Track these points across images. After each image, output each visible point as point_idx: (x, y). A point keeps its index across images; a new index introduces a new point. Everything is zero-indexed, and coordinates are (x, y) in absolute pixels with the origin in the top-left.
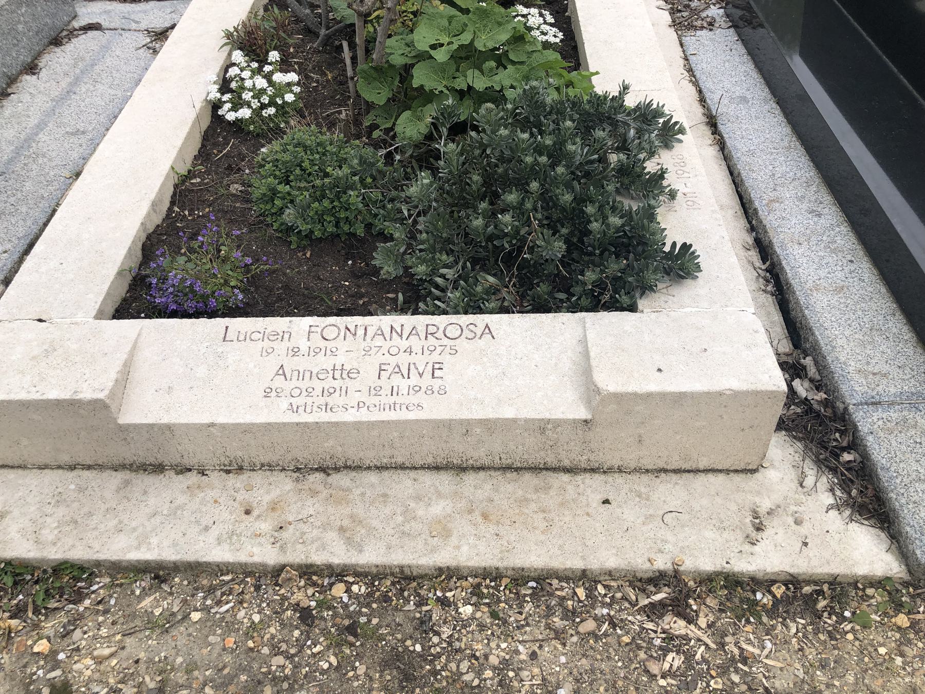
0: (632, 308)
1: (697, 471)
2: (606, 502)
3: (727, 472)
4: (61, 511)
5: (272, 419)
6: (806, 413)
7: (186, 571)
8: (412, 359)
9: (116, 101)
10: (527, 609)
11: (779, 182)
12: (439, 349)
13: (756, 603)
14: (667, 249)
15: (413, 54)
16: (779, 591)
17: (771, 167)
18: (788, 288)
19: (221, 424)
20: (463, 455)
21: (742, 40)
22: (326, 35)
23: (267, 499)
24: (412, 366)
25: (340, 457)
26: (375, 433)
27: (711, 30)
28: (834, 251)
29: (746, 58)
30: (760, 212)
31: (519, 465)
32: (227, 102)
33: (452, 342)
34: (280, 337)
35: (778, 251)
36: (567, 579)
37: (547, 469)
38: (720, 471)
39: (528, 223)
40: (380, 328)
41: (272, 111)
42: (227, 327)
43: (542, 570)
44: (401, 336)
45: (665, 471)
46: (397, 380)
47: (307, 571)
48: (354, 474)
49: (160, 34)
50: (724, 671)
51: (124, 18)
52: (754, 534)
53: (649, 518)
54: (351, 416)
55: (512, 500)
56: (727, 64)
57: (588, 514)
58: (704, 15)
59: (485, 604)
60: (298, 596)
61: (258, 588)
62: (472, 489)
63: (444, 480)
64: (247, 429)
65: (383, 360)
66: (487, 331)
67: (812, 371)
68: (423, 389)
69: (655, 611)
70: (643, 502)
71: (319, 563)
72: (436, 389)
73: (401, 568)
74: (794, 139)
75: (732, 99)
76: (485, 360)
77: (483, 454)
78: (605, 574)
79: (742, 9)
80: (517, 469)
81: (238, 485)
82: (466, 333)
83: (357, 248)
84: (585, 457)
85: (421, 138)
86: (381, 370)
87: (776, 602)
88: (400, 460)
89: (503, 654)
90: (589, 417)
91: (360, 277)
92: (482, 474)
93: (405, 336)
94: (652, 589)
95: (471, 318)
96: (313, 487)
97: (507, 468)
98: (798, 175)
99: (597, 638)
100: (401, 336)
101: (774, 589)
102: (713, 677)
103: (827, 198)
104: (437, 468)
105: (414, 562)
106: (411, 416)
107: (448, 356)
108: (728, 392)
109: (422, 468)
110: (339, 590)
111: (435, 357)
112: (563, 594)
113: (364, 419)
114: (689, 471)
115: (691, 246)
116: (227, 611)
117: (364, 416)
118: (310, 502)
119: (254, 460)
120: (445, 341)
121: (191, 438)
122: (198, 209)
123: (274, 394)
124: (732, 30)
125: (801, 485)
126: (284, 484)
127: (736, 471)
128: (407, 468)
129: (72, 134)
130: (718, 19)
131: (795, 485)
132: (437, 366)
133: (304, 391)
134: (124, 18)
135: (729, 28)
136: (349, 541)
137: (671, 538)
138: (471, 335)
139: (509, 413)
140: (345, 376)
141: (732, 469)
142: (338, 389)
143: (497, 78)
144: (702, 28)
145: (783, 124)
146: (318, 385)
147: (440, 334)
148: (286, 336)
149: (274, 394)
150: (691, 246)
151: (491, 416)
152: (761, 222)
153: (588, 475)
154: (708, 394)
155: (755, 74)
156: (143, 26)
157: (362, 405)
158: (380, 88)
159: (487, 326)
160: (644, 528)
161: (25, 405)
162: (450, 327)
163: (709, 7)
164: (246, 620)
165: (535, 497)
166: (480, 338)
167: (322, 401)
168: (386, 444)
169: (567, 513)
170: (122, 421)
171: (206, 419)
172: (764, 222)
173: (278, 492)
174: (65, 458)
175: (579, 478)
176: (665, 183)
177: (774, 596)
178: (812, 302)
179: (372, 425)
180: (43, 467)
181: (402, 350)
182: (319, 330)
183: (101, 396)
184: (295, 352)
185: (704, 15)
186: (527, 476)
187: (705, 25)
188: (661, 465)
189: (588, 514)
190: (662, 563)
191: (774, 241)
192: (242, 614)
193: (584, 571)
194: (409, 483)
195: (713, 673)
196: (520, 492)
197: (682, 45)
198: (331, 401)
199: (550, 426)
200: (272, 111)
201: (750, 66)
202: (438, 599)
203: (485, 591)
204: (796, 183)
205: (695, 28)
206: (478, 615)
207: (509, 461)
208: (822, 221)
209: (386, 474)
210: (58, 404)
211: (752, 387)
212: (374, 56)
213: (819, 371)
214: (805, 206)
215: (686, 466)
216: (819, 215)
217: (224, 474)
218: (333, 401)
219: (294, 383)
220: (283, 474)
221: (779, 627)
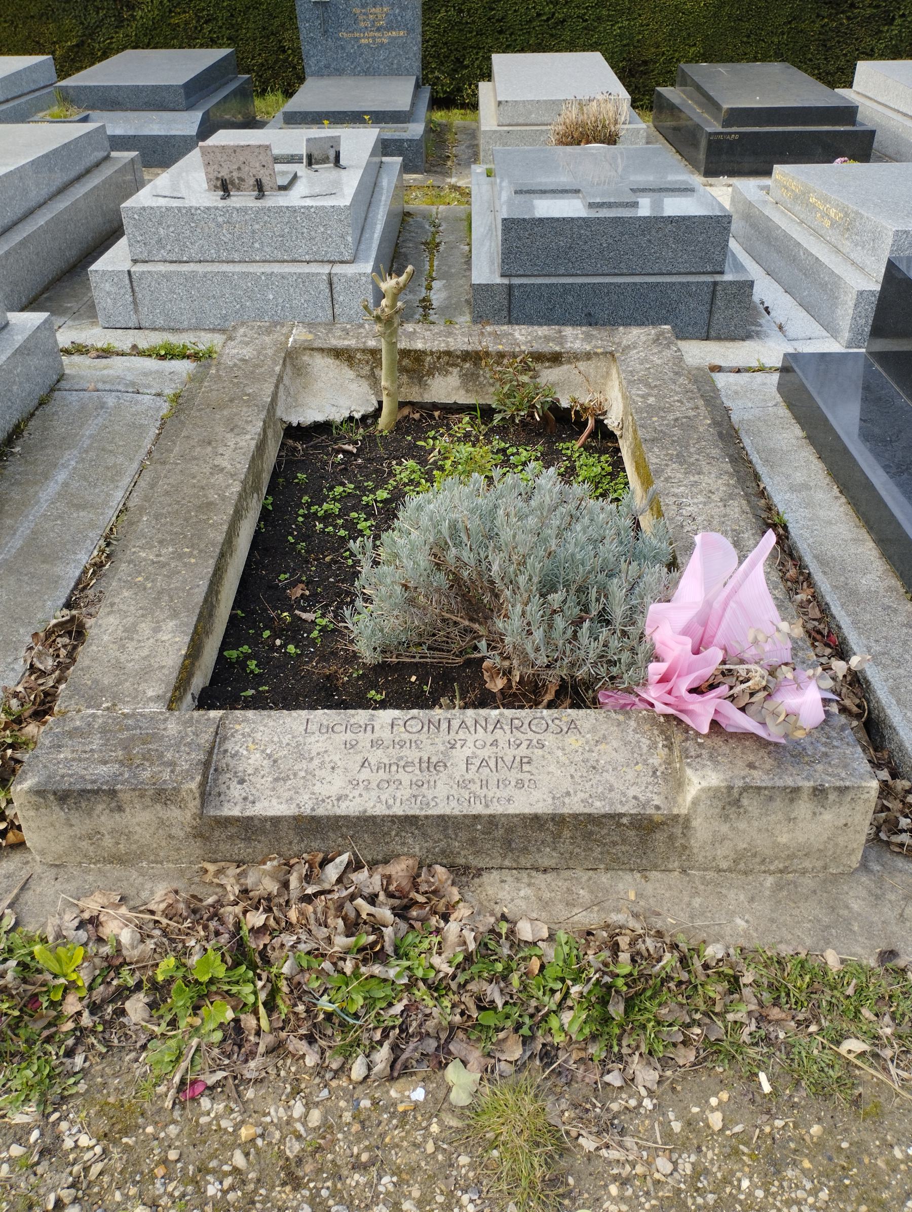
33: (539, 736)
132: (525, 760)
146: (405, 778)
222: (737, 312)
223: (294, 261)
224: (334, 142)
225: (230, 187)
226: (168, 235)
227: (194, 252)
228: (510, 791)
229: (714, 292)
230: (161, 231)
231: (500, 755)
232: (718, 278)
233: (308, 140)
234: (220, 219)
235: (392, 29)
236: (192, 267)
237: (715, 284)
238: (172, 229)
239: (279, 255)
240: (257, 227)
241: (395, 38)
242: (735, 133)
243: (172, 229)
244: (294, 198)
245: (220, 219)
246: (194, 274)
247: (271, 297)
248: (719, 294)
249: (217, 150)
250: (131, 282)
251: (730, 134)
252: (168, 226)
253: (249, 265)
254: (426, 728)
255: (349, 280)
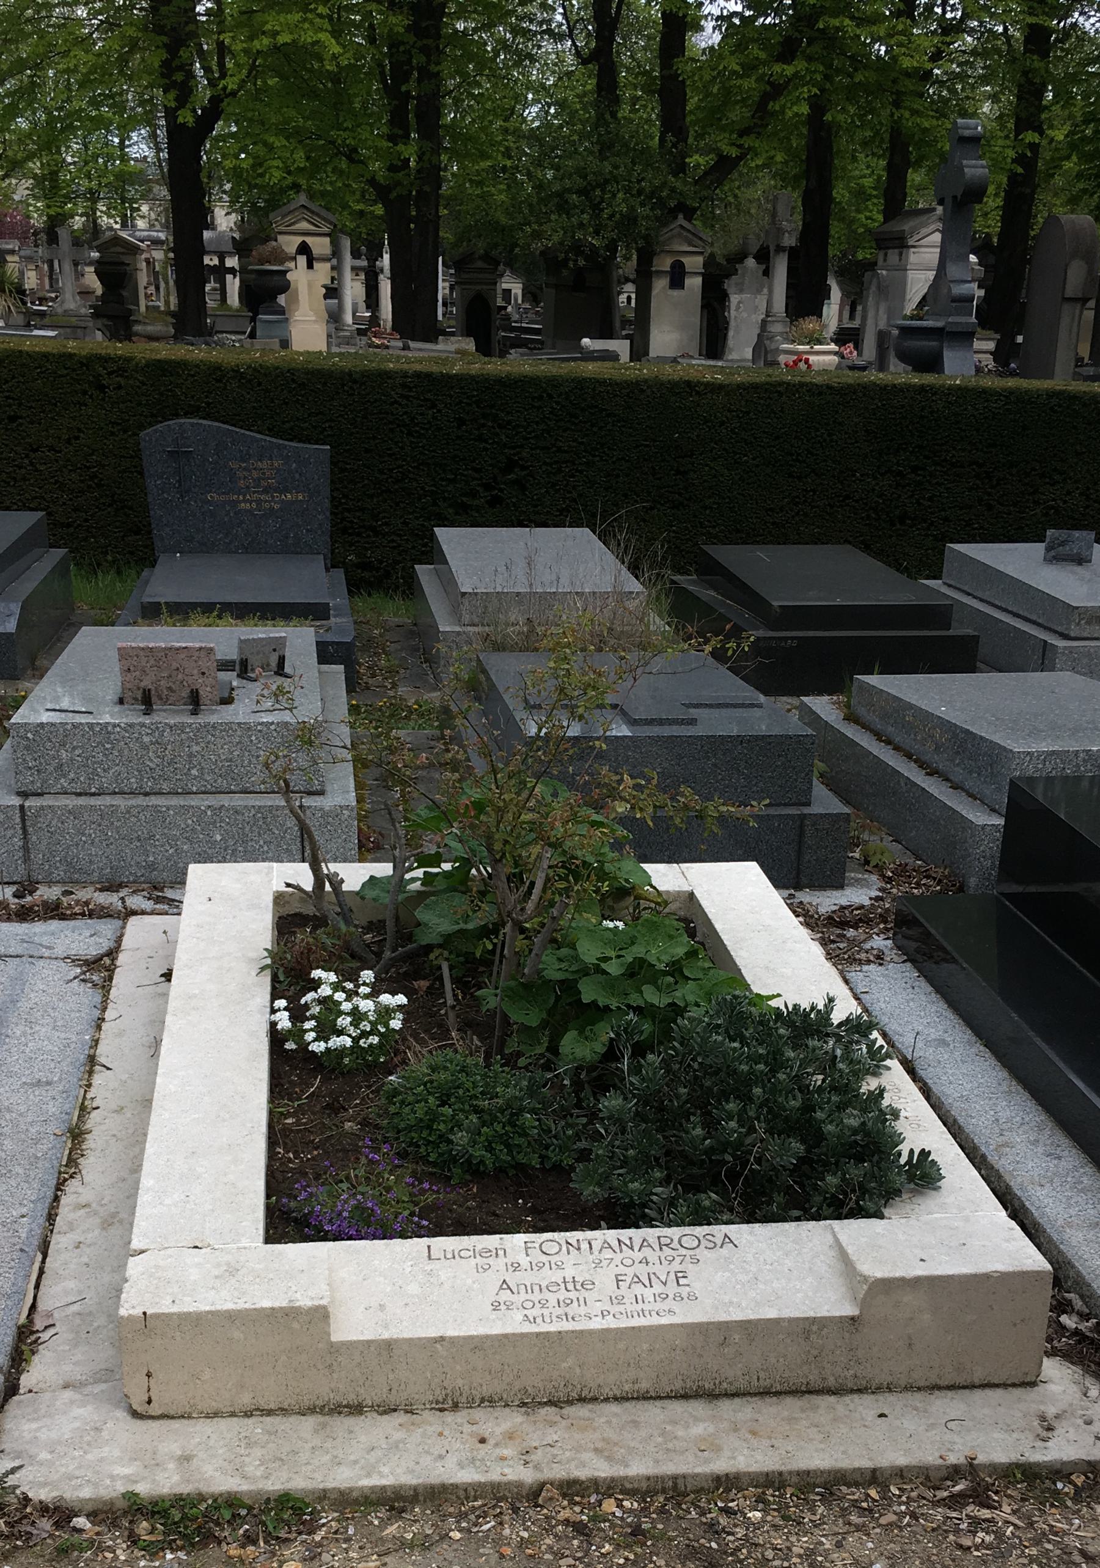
0: (881, 1217)
1: (972, 1387)
2: (882, 1415)
3: (1005, 1386)
4: (258, 1452)
5: (509, 1330)
6: (1079, 1342)
7: (425, 1501)
8: (650, 1269)
9: (73, 1046)
10: (820, 1511)
11: (1005, 1126)
12: (678, 1260)
13: (1058, 1492)
14: (903, 1160)
15: (574, 968)
16: (1079, 1480)
17: (992, 1113)
18: (1037, 1231)
19: (451, 1338)
20: (717, 1376)
21: (925, 977)
22: (391, 959)
23: (498, 1431)
24: (652, 1276)
25: (575, 1383)
26: (621, 1346)
27: (881, 964)
28: (1082, 1191)
29: (934, 996)
30: (990, 1157)
31: (778, 1388)
32: (311, 1030)
33: (691, 1252)
34: (494, 1253)
35: (1019, 1193)
36: (857, 1485)
37: (810, 1392)
38: (997, 1386)
39: (752, 1130)
40: (605, 1242)
41: (375, 1040)
42: (429, 1247)
43: (829, 1472)
44: (632, 1248)
45: (939, 1388)
46: (638, 1289)
47: (571, 1489)
48: (590, 1406)
49: (94, 963)
50: (1037, 1542)
51: (23, 941)
52: (1044, 1434)
53: (932, 1426)
54: (597, 1324)
55: (778, 1419)
56: (911, 1004)
57: (865, 1426)
58: (867, 946)
59: (774, 1510)
60: (565, 1514)
61: (515, 1510)
62: (732, 1413)
63: (697, 1407)
64: (478, 1345)
65: (618, 1271)
66: (727, 1240)
67: (1078, 1304)
68: (671, 1296)
69: (956, 1501)
70: (921, 1414)
71: (583, 1478)
72: (684, 1295)
73: (675, 1478)
74: (1014, 1083)
75: (927, 1043)
76: (732, 1267)
77: (740, 1373)
78: (896, 1475)
79: (916, 941)
80: (778, 1394)
81: (459, 1420)
82: (704, 1243)
83: (526, 1186)
84: (852, 1372)
85: (596, 1058)
86: (618, 1281)
87: (1078, 1490)
88: (644, 1385)
89: (805, 1545)
90: (855, 1312)
91: (543, 1212)
92: (737, 1400)
93: (636, 1248)
94: (949, 1483)
95: (706, 1229)
96: (547, 1418)
97: (764, 1393)
98: (1027, 1119)
99: (901, 1528)
100: (632, 1248)
101: (1073, 1477)
102: (1026, 1547)
103: (1065, 1141)
104: (685, 1397)
105: (690, 1471)
106: (665, 1321)
107: (706, 1252)
108: (995, 1275)
109: (668, 1397)
110: (609, 1506)
111: (676, 1266)
112: (856, 1497)
113: (613, 1326)
114: (964, 1387)
115: (929, 1152)
116: (489, 1530)
117: (610, 1323)
118: (551, 1430)
119: (474, 1392)
120: (684, 1252)
121: (410, 1360)
122: (303, 1152)
123: (503, 1307)
124: (909, 964)
125: (1085, 1395)
126: (513, 1419)
127: (1014, 1385)
128: (651, 1398)
129: (33, 1085)
130: (887, 952)
131: (1079, 1395)
132: (680, 1275)
133: (537, 1303)
134: (23, 941)
135: (904, 962)
136: (609, 1459)
137: (957, 1439)
138: (712, 1245)
139: (772, 1314)
140: (579, 1287)
141: (1009, 1382)
142: (575, 1300)
143: (678, 994)
144: (869, 962)
145: (997, 1068)
146: (552, 1299)
147: (675, 1245)
148: (501, 1253)
149: (503, 1307)
150: (929, 1152)
151: (752, 1317)
152: (993, 1167)
153: (856, 1396)
154: (975, 1276)
155: (949, 1014)
156: (60, 951)
157: (605, 1313)
158: (528, 1009)
159: (726, 1236)
160: (929, 1434)
161: (231, 1317)
162: (685, 1238)
163: (871, 937)
164: (514, 1537)
165: (804, 1416)
166: (721, 1247)
167: (559, 1311)
168: (632, 1361)
169: (841, 1426)
170: (334, 1338)
171: (433, 1333)
172: (996, 1166)
173: (509, 1424)
174: (246, 1400)
175: (847, 1399)
176: (885, 1103)
177: (1075, 1485)
178: (1066, 1237)
179: (620, 1333)
180: (216, 1415)
181: (637, 1262)
182: (537, 1246)
183: (322, 1302)
184: (516, 1267)
185: (867, 946)
186: (789, 1400)
187: (872, 958)
188: (933, 1379)
189: (865, 1426)
190: (955, 1458)
191: (1012, 1184)
192: (507, 1532)
193: (874, 1471)
194: (658, 1411)
195: (1026, 1543)
196: (786, 1413)
197: (847, 981)
198: (570, 1311)
199: (815, 1328)
200: (375, 1040)
201: (942, 1006)
202: (721, 1509)
203: (771, 1499)
204: (1026, 1127)
205: (860, 962)
206: (769, 1518)
207: (768, 1383)
208: (1063, 1163)
209: (627, 1405)
210: (271, 1314)
211: (1019, 1269)
212: (526, 971)
213: (1086, 1303)
214: (1040, 1150)
215: (960, 1380)
216: (1059, 1158)
217: (438, 1413)
218: (571, 1311)
219: (523, 1296)
220: (507, 1409)
221: (1085, 1509)
222: (832, 852)
223: (245, 792)
224: (278, 645)
225: (154, 699)
226: (72, 760)
227: (106, 781)
228: (669, 1304)
229: (801, 834)
230: (64, 754)
231: (651, 1271)
232: (806, 810)
233: (241, 641)
234: (146, 739)
235: (286, 490)
236: (108, 800)
237: (803, 817)
238: (77, 752)
239: (222, 783)
240: (195, 748)
241: (292, 502)
242: (792, 638)
243: (77, 752)
244: (241, 712)
245: (146, 739)
246: (114, 809)
247: (218, 838)
248: (809, 831)
249: (142, 653)
250: (23, 820)
251: (786, 639)
252: (74, 748)
253: (181, 797)
254: (564, 1248)
255: (325, 814)
